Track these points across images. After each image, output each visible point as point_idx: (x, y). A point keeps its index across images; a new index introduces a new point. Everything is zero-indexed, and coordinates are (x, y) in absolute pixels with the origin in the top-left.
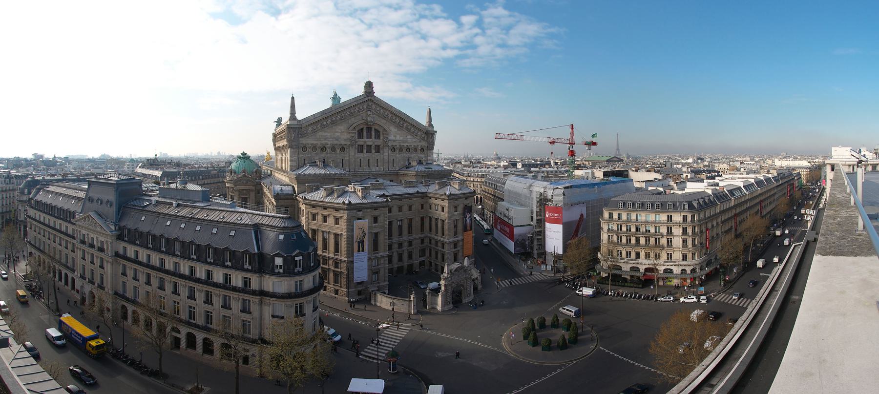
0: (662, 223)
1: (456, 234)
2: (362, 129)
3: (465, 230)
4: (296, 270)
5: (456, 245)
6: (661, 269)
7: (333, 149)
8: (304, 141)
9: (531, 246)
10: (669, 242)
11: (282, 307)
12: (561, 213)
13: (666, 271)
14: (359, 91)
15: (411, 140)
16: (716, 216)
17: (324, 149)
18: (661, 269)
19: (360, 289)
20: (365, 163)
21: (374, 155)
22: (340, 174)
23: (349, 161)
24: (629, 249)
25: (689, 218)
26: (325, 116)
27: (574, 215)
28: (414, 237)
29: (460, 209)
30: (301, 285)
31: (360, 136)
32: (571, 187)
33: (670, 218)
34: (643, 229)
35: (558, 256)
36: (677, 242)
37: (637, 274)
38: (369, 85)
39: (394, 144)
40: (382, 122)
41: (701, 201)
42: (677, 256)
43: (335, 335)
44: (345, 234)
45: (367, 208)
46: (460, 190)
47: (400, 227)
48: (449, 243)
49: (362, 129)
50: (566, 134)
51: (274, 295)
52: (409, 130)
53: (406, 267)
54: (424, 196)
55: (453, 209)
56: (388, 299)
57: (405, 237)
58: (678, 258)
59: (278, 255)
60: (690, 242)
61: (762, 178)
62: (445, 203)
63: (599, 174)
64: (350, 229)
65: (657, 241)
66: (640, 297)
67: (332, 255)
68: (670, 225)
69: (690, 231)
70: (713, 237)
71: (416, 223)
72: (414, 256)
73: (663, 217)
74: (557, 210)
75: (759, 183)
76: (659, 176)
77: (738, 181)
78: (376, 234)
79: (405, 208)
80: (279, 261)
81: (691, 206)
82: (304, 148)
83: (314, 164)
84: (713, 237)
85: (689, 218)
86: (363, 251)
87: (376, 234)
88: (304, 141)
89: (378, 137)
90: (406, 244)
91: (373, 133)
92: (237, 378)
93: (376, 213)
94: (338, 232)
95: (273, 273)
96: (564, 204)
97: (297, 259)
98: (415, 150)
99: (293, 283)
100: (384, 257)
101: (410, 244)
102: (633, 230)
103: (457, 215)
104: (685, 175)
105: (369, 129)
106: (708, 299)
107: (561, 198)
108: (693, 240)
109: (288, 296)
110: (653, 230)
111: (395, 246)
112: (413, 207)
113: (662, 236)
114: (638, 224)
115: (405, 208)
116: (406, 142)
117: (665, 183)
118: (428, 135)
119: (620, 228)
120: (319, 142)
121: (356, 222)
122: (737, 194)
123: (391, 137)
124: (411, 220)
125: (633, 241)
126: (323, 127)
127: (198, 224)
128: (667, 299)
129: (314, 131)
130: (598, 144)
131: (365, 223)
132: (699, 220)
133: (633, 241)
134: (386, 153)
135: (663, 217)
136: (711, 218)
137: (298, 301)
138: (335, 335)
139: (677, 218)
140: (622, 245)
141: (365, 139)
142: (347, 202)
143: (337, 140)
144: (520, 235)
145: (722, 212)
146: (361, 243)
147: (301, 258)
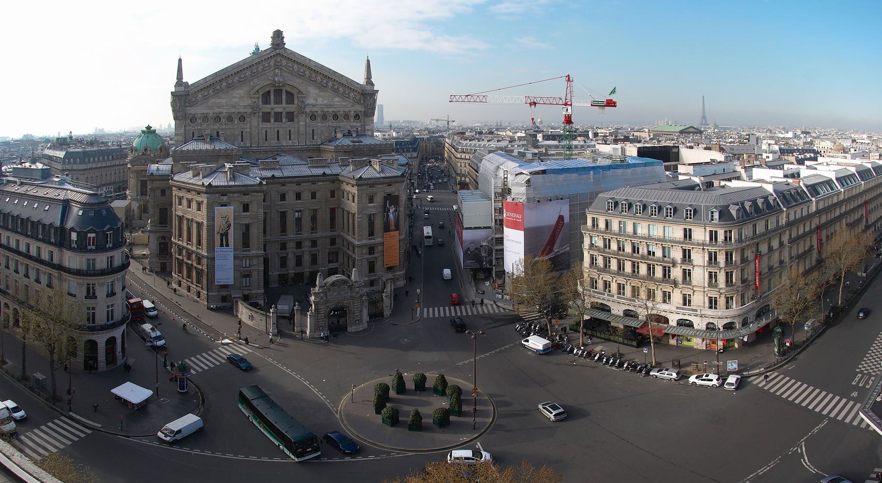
0: (674, 242)
1: (371, 234)
2: (269, 92)
3: (387, 228)
4: (89, 248)
5: (371, 250)
6: (673, 320)
7: (230, 119)
8: (192, 110)
9: (486, 262)
10: (687, 274)
11: (74, 284)
12: (522, 213)
13: (681, 323)
14: (266, 44)
15: (338, 104)
16: (779, 230)
17: (217, 118)
18: (673, 320)
19: (224, 294)
20: (272, 135)
21: (285, 126)
22: (226, 150)
23: (250, 133)
24: (621, 280)
25: (721, 237)
26: (218, 79)
27: (548, 216)
28: (320, 234)
29: (379, 199)
30: (94, 265)
31: (266, 101)
32: (544, 172)
33: (688, 234)
34: (643, 250)
35: (517, 280)
36: (699, 276)
37: (633, 323)
38: (278, 36)
39: (314, 109)
40: (297, 82)
41: (747, 205)
42: (699, 299)
43: (159, 338)
44: (205, 223)
45: (233, 193)
46: (382, 171)
47: (299, 220)
48: (359, 246)
49: (269, 92)
50: (559, 90)
51: (69, 271)
52: (336, 91)
53: (307, 274)
54: (335, 179)
55: (365, 199)
56: (248, 311)
57: (306, 234)
58: (697, 304)
59: (91, 231)
60: (721, 278)
61: (869, 166)
62: (355, 190)
63: (632, 150)
64: (211, 217)
65: (666, 272)
66: (621, 365)
67: (194, 248)
68: (687, 247)
69: (721, 258)
70: (771, 268)
71: (324, 216)
72: (319, 261)
73: (676, 232)
74: (516, 207)
75: (864, 173)
76: (720, 157)
77: (827, 168)
78: (247, 226)
79: (306, 196)
80: (74, 236)
81: (724, 214)
82: (193, 119)
83: (201, 138)
84: (771, 268)
85: (721, 237)
86: (227, 245)
87: (247, 226)
88: (192, 110)
89: (290, 101)
90: (307, 244)
91: (284, 97)
92: (24, 348)
93: (246, 199)
94: (199, 220)
95: (70, 249)
96: (528, 199)
97: (89, 235)
98: (347, 116)
99: (84, 260)
100: (257, 256)
101: (314, 243)
102: (628, 249)
103: (374, 208)
104: (764, 156)
105: (278, 92)
106: (741, 384)
107: (523, 189)
108: (729, 276)
109: (78, 273)
110: (659, 253)
111: (291, 246)
112: (317, 195)
113: (674, 264)
114: (636, 241)
115: (306, 196)
116: (332, 106)
117: (729, 167)
118: (365, 97)
119: (607, 245)
120: (211, 112)
121: (218, 209)
122: (823, 192)
123: (310, 101)
124: (315, 211)
125: (628, 268)
126: (217, 92)
127: (7, 196)
128: (665, 375)
129: (206, 98)
130: (617, 104)
131: (229, 211)
132: (740, 240)
133: (628, 268)
134: (302, 122)
135: (676, 232)
136: (768, 234)
137: (91, 280)
138: (159, 338)
139: (700, 234)
140: (655, 281)
141: (272, 105)
142: (206, 184)
143: (234, 107)
144: (472, 242)
145: (790, 224)
146: (224, 235)
147: (94, 235)
